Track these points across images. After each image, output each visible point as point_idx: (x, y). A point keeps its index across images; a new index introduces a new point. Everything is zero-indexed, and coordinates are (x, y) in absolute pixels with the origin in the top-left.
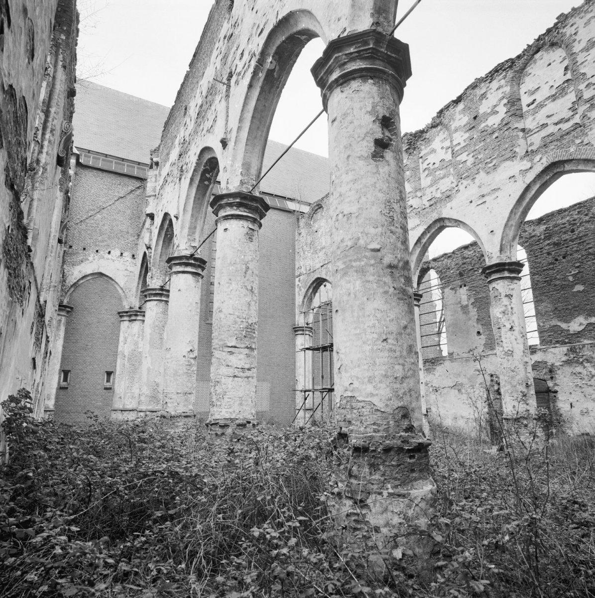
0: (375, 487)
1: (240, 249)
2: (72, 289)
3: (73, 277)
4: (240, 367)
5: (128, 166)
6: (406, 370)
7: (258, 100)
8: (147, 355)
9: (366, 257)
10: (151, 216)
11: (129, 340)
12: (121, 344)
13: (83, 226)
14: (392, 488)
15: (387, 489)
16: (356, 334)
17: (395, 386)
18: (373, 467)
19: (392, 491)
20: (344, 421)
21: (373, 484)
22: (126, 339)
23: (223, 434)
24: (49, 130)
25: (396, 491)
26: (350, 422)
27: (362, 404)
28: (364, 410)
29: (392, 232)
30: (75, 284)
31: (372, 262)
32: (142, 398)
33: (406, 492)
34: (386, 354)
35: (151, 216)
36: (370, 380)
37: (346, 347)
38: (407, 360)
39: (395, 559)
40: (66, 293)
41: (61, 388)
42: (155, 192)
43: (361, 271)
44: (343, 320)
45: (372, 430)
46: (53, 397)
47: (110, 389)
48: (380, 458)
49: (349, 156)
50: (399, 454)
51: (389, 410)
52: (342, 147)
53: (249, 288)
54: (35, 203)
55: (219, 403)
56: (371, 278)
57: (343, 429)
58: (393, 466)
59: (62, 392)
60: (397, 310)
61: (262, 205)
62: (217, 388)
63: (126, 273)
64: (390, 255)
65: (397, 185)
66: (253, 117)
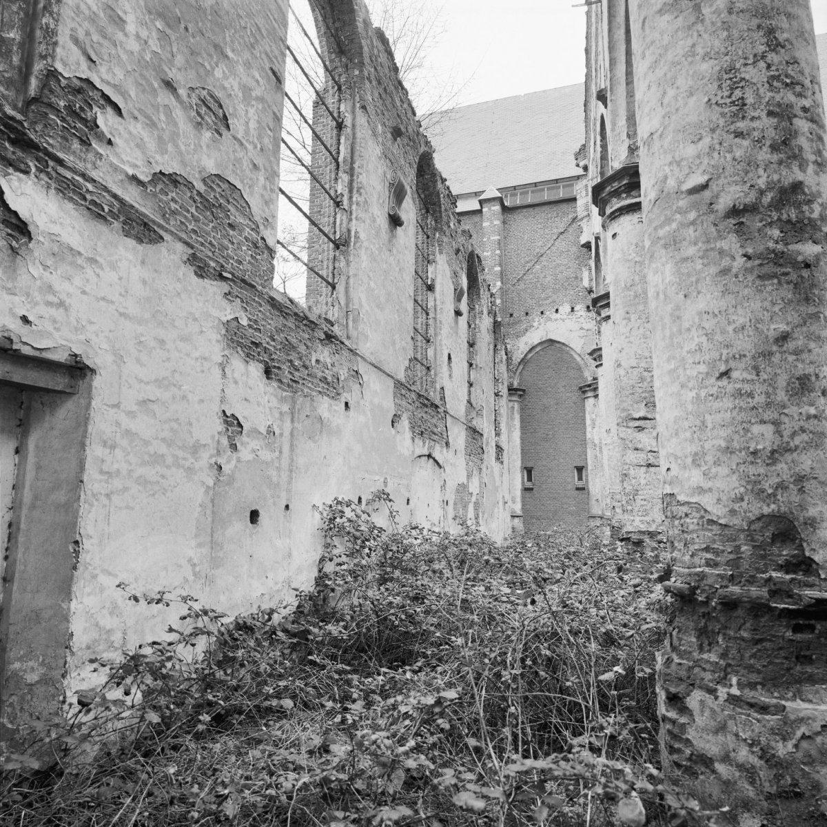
1: (637, 259)
2: (521, 367)
3: (520, 352)
6: (786, 433)
9: (679, 211)
12: (589, 429)
13: (522, 286)
14: (740, 685)
17: (752, 470)
18: (706, 637)
21: (704, 670)
22: (593, 421)
25: (749, 694)
27: (685, 509)
28: (688, 520)
31: (692, 215)
33: (775, 701)
34: (728, 403)
36: (697, 460)
40: (515, 373)
41: (526, 490)
43: (673, 243)
45: (703, 561)
46: (519, 500)
51: (736, 521)
54: (351, 281)
56: (691, 251)
58: (743, 639)
59: (528, 494)
60: (756, 305)
62: (625, 484)
63: (582, 333)
64: (733, 188)
65: (755, 22)
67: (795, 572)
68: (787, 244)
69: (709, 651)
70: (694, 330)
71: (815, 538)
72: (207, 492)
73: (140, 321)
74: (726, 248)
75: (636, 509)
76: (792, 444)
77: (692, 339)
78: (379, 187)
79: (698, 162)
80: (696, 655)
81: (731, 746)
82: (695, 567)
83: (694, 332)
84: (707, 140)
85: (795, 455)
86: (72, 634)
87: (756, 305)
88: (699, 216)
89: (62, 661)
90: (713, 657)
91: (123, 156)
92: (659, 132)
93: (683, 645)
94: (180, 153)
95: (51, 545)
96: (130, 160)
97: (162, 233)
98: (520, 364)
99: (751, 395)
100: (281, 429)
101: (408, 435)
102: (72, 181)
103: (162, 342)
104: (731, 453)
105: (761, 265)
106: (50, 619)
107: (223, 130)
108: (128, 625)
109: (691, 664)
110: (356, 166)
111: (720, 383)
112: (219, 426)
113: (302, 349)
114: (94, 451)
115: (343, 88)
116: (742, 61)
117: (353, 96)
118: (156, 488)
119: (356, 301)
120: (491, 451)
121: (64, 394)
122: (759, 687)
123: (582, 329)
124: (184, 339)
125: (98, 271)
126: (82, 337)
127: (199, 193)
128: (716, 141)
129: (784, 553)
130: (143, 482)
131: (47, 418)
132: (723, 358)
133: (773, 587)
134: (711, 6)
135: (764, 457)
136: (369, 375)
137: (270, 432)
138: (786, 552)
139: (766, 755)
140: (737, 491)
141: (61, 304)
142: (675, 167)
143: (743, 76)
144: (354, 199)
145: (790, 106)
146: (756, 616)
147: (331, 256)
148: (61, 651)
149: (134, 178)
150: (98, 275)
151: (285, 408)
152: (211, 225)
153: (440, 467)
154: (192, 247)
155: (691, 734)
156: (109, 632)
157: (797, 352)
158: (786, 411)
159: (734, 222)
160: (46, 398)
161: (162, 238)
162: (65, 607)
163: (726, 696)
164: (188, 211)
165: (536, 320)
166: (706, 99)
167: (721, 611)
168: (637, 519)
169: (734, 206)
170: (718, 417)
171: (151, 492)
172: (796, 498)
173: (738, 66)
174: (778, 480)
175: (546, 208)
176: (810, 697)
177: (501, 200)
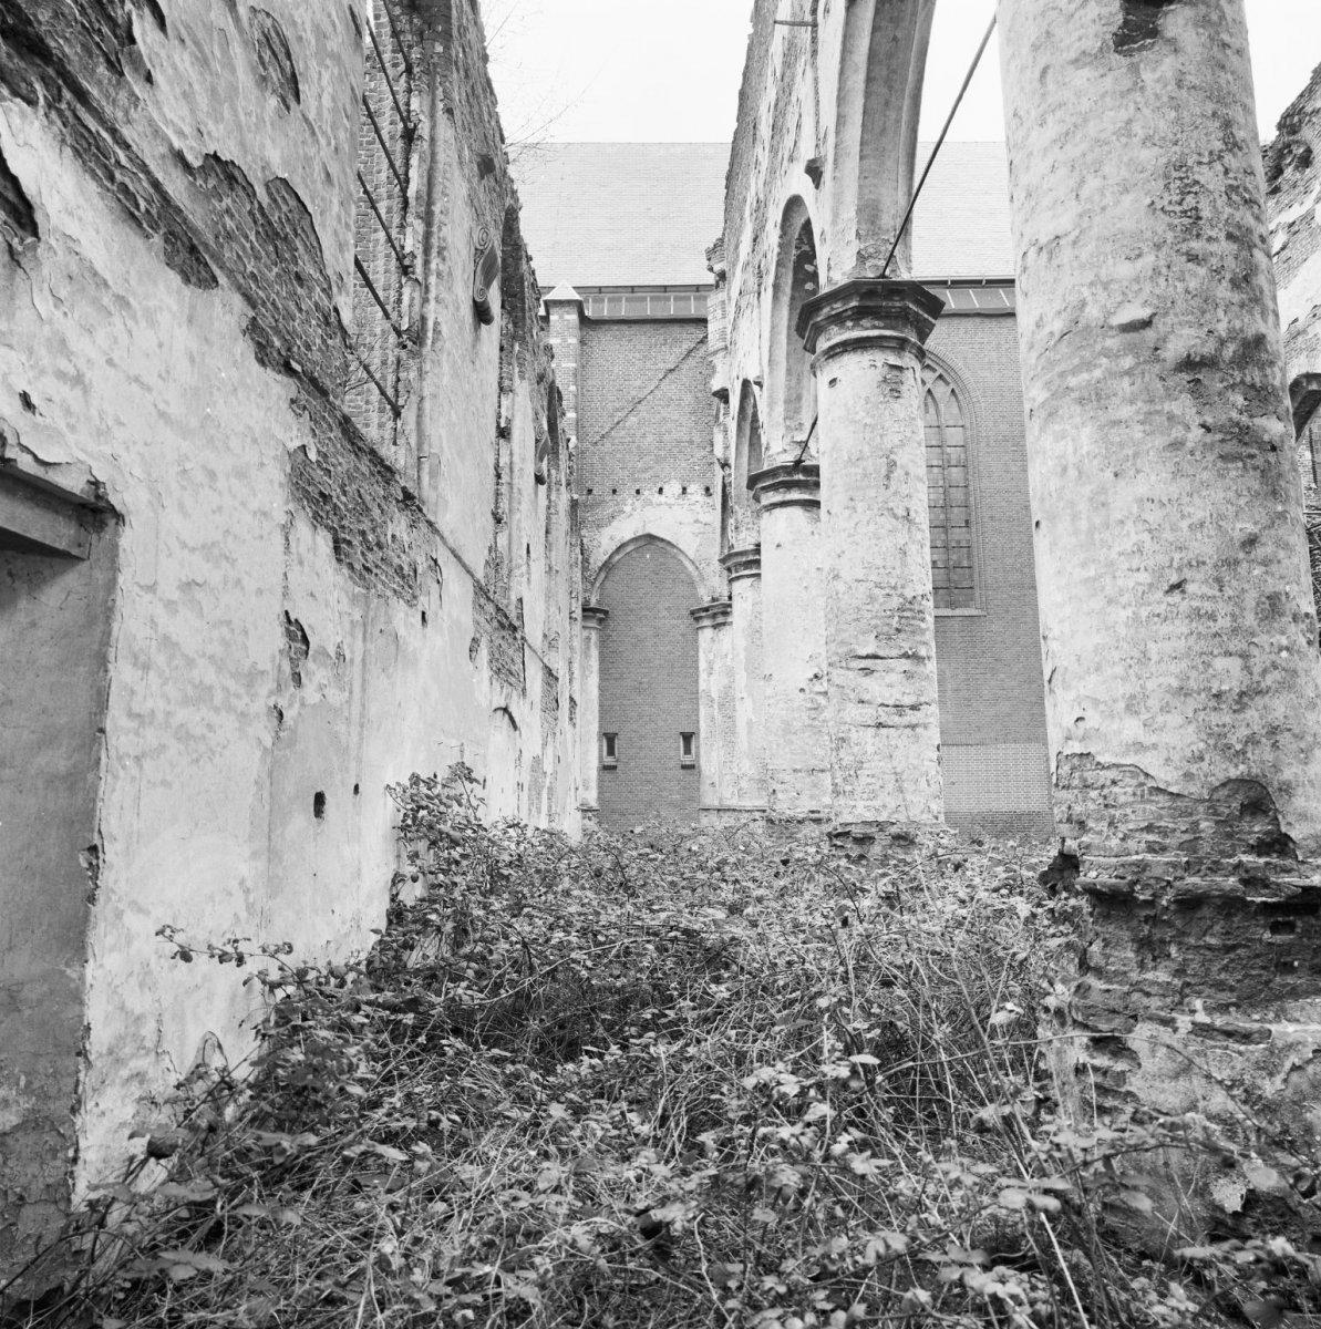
0: (1155, 1003)
1: (868, 420)
2: (603, 575)
4: (891, 702)
5: (676, 299)
6: (1257, 670)
7: (875, 29)
8: (745, 695)
9: (1106, 353)
10: (723, 395)
11: (716, 667)
12: (703, 676)
13: (608, 446)
14: (1209, 1010)
15: (1193, 1012)
16: (1087, 580)
17: (1215, 719)
18: (1150, 949)
19: (1207, 1020)
20: (1069, 820)
21: (1148, 995)
23: (862, 857)
24: (434, 251)
25: (1219, 1021)
26: (1082, 824)
28: (1116, 789)
29: (1193, 258)
30: (605, 564)
31: (1128, 362)
32: (744, 784)
33: (1256, 1026)
34: (1182, 627)
35: (723, 395)
37: (1061, 621)
38: (1262, 639)
39: (1221, 1209)
40: (593, 584)
41: (606, 768)
42: (724, 339)
43: (1096, 397)
44: (1054, 544)
45: (1143, 845)
46: (594, 784)
47: (692, 767)
48: (1169, 924)
49: (1044, 71)
50: (1228, 916)
51: (1194, 789)
52: (1025, 50)
53: (901, 512)
54: (427, 405)
55: (848, 788)
56: (1126, 412)
57: (1068, 842)
58: (1209, 948)
59: (608, 776)
60: (1218, 495)
61: (917, 302)
62: (842, 754)
63: (697, 528)
64: (1186, 331)
65: (1210, 107)
66: (869, 80)
67: (1268, 855)
68: (1251, 417)
69: (1155, 968)
70: (1129, 524)
71: (1291, 809)
72: (263, 760)
73: (185, 432)
74: (1178, 412)
75: (859, 789)
76: (1263, 685)
77: (1128, 534)
78: (464, 252)
79: (1136, 287)
80: (1134, 976)
81: (1199, 1093)
82: (1129, 854)
83: (1129, 525)
84: (1149, 259)
85: (1267, 698)
86: (88, 1028)
87: (1218, 495)
88: (1139, 364)
89: (70, 1082)
90: (1162, 976)
91: (166, 110)
92: (1072, 237)
93: (1113, 964)
94: (239, 126)
95: (38, 855)
96: (176, 120)
97: (217, 272)
98: (601, 569)
99: (1212, 617)
100: (352, 652)
101: (486, 673)
102: (96, 137)
103: (212, 475)
104: (1186, 695)
105: (1223, 441)
106: (40, 1002)
107: (293, 104)
108: (165, 1004)
109: (1126, 988)
110: (437, 209)
111: (1169, 599)
112: (279, 640)
113: (376, 512)
114: (122, 673)
115: (416, 70)
116: (1195, 157)
117: (432, 88)
118: (202, 748)
119: (434, 440)
120: (565, 704)
121: (62, 558)
122: (1232, 1009)
123: (697, 521)
124: (241, 474)
125: (130, 323)
126: (107, 450)
127: (261, 207)
128: (1162, 262)
129: (1256, 829)
130: (184, 735)
131: (23, 604)
132: (1175, 564)
133: (1245, 876)
134: (1154, 70)
135: (1230, 701)
136: (450, 570)
137: (340, 656)
138: (1258, 828)
139: (1251, 1097)
140: (1194, 748)
141: (78, 380)
142: (1099, 289)
143: (1197, 177)
144: (433, 266)
145: (1249, 231)
146: (1228, 916)
147: (391, 359)
148: (69, 1062)
149: (179, 157)
150: (130, 332)
151: (357, 616)
152: (275, 270)
153: (515, 727)
154: (254, 307)
155: (1135, 1084)
156: (139, 1019)
157: (1266, 563)
158: (1255, 640)
159: (1188, 378)
160: (56, 561)
161: (214, 279)
162: (74, 976)
163: (1190, 1027)
164: (246, 237)
165: (629, 503)
166: (1148, 201)
167: (1175, 912)
168: (861, 804)
169: (1189, 356)
170: (1167, 647)
171: (195, 756)
172: (1269, 756)
173: (1190, 163)
174: (1247, 732)
175: (647, 327)
176: (1297, 1015)
177: (579, 306)
